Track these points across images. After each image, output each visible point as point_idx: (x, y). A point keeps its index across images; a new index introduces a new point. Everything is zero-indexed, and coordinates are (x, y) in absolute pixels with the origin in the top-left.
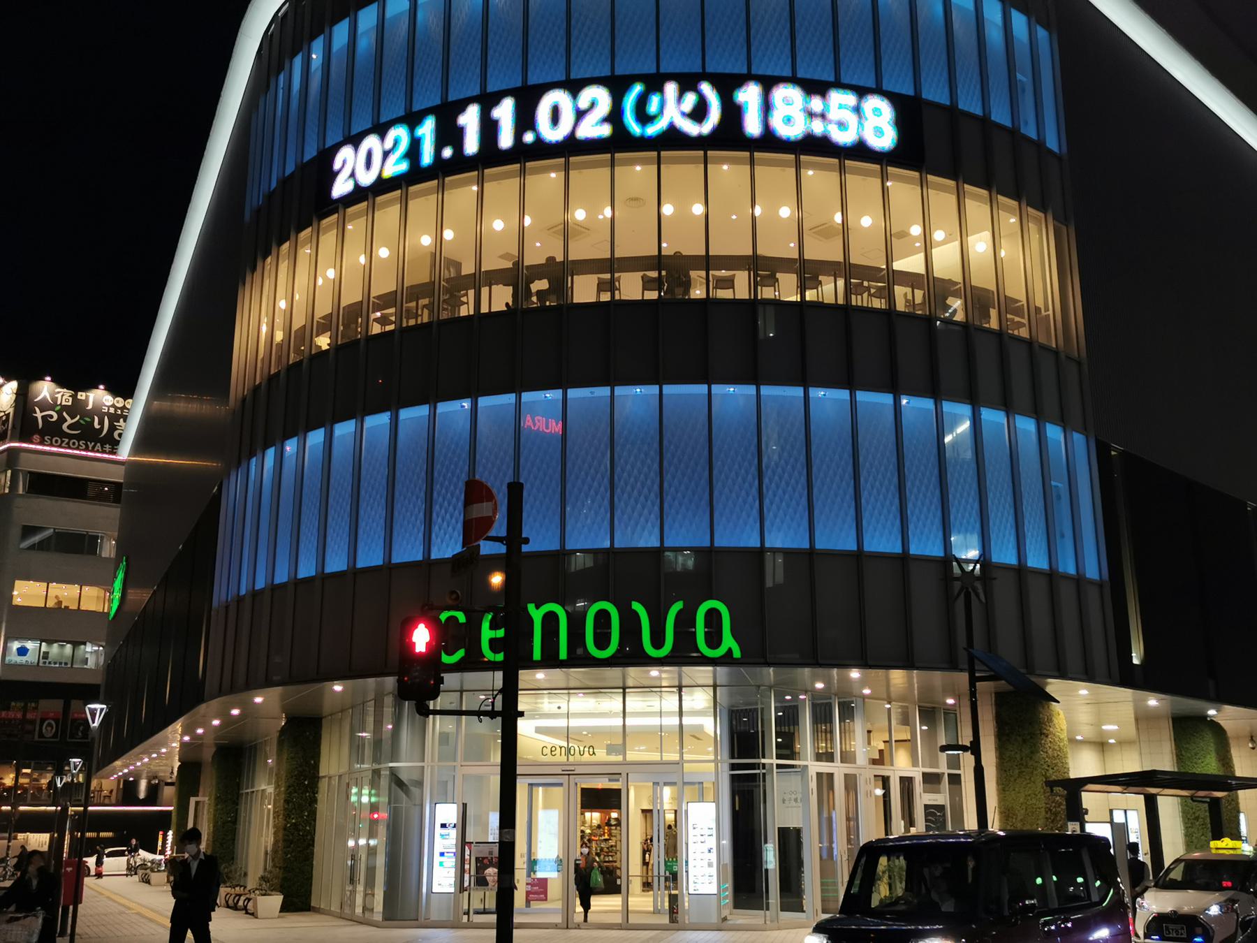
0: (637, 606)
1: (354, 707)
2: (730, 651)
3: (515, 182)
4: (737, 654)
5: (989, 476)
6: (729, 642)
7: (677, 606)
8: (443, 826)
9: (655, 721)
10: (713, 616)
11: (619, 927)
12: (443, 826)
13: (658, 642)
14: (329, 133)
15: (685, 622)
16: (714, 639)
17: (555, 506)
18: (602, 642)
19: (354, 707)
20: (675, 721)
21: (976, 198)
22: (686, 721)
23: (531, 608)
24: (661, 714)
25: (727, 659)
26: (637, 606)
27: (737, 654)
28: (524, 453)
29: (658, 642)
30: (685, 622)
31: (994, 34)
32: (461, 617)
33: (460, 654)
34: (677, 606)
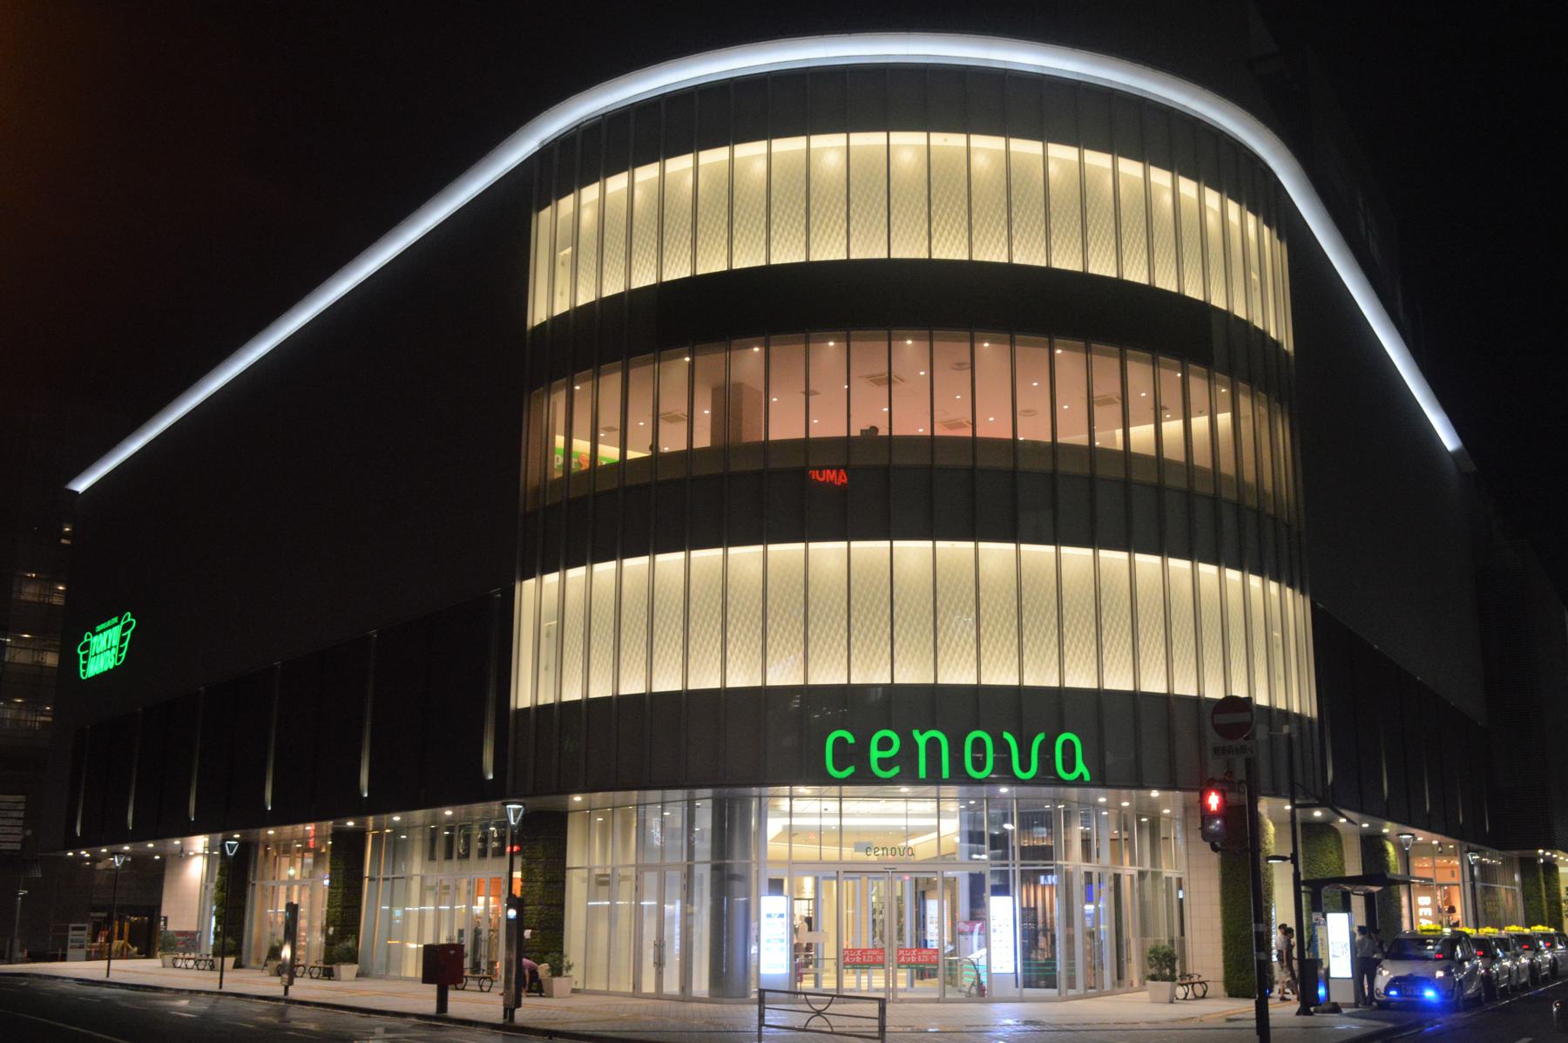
0: (1007, 736)
1: (590, 810)
2: (1081, 775)
3: (802, 347)
4: (1087, 777)
5: (1174, 623)
6: (1081, 768)
7: (1040, 738)
8: (769, 916)
9: (815, 822)
10: (1068, 745)
11: (937, 1001)
12: (769, 916)
13: (1025, 767)
14: (581, 290)
15: (1047, 749)
16: (1070, 766)
17: (799, 644)
18: (979, 765)
19: (590, 810)
20: (836, 821)
21: (1198, 375)
22: (846, 822)
23: (916, 733)
24: (821, 815)
25: (1079, 782)
26: (1007, 736)
27: (1087, 777)
28: (731, 591)
29: (1025, 767)
30: (1047, 749)
31: (1213, 221)
32: (851, 739)
33: (850, 770)
34: (1040, 738)
